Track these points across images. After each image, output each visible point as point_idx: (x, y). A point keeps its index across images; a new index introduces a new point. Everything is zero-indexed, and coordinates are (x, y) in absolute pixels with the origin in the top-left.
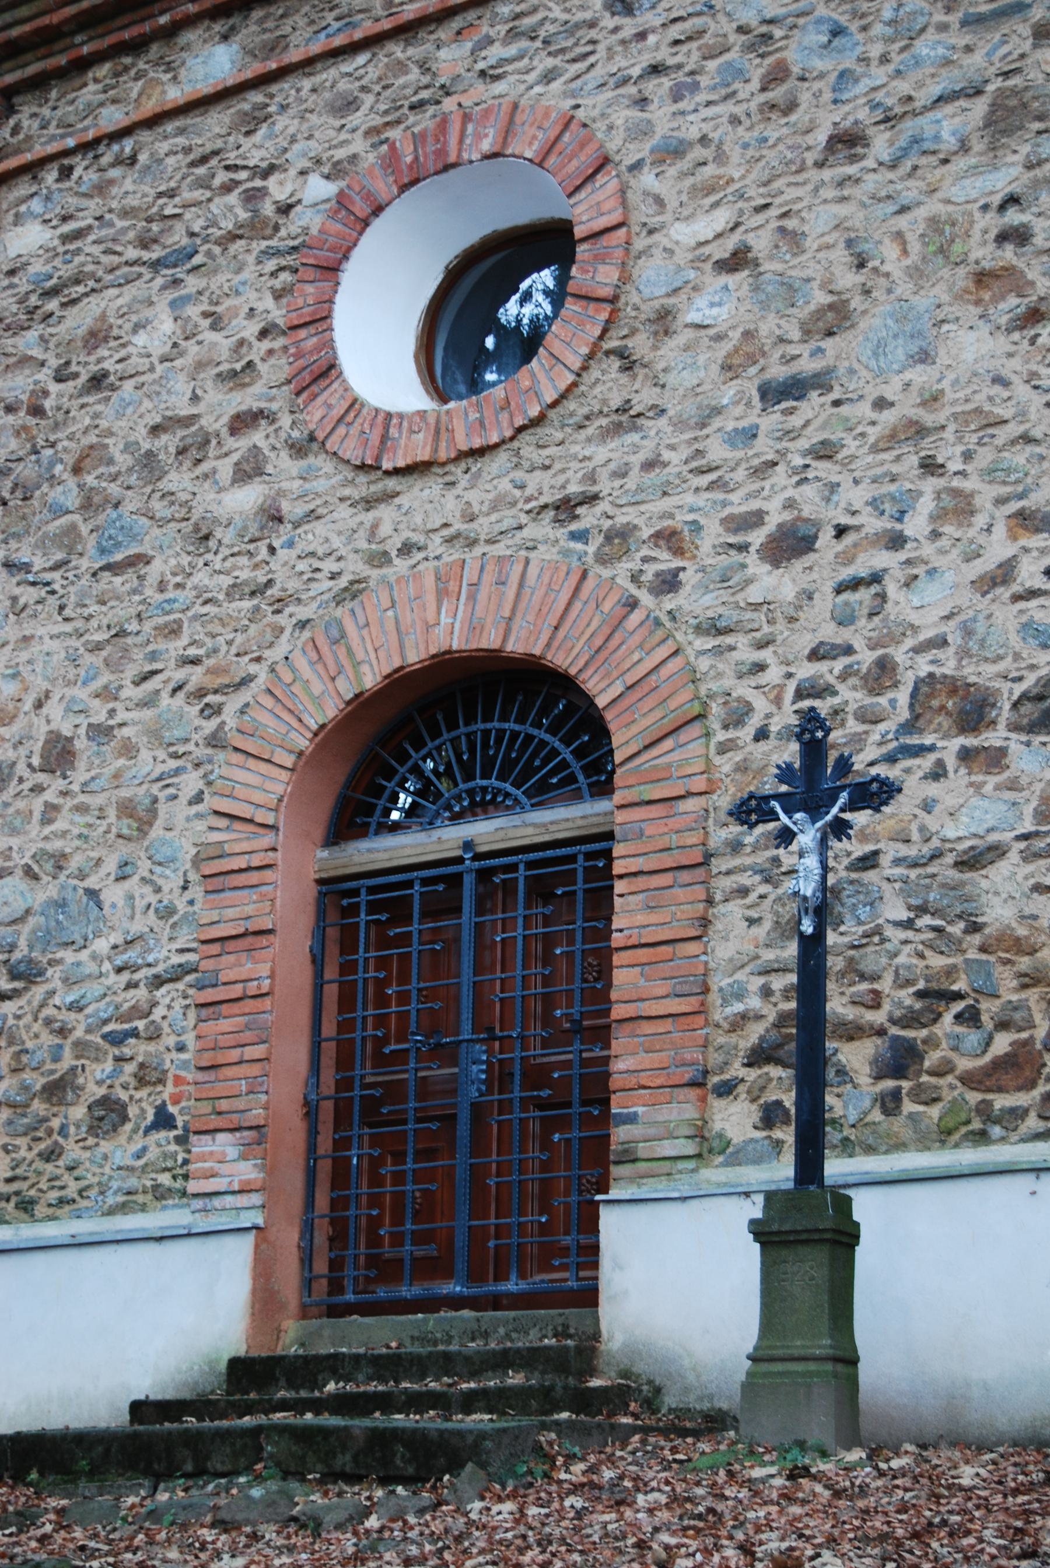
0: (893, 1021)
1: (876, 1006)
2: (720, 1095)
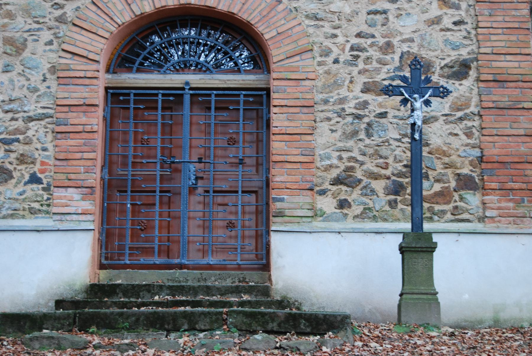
0: (393, 174)
1: (386, 168)
2: (320, 195)
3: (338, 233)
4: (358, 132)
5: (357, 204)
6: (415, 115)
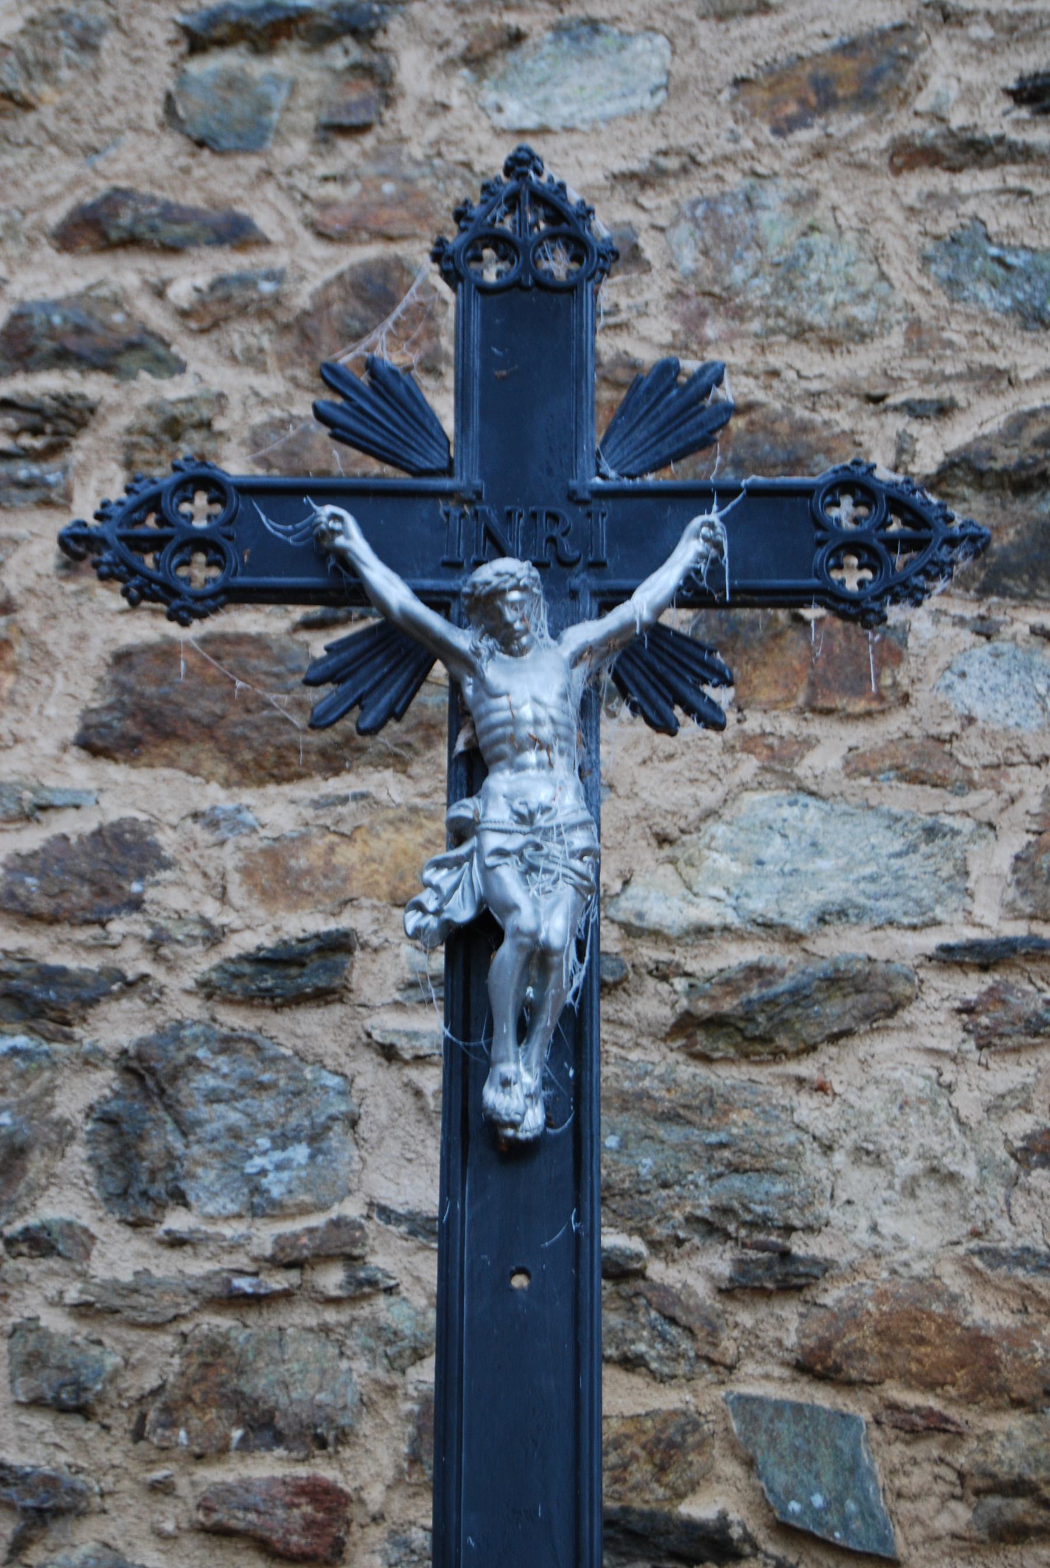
6: (498, 813)
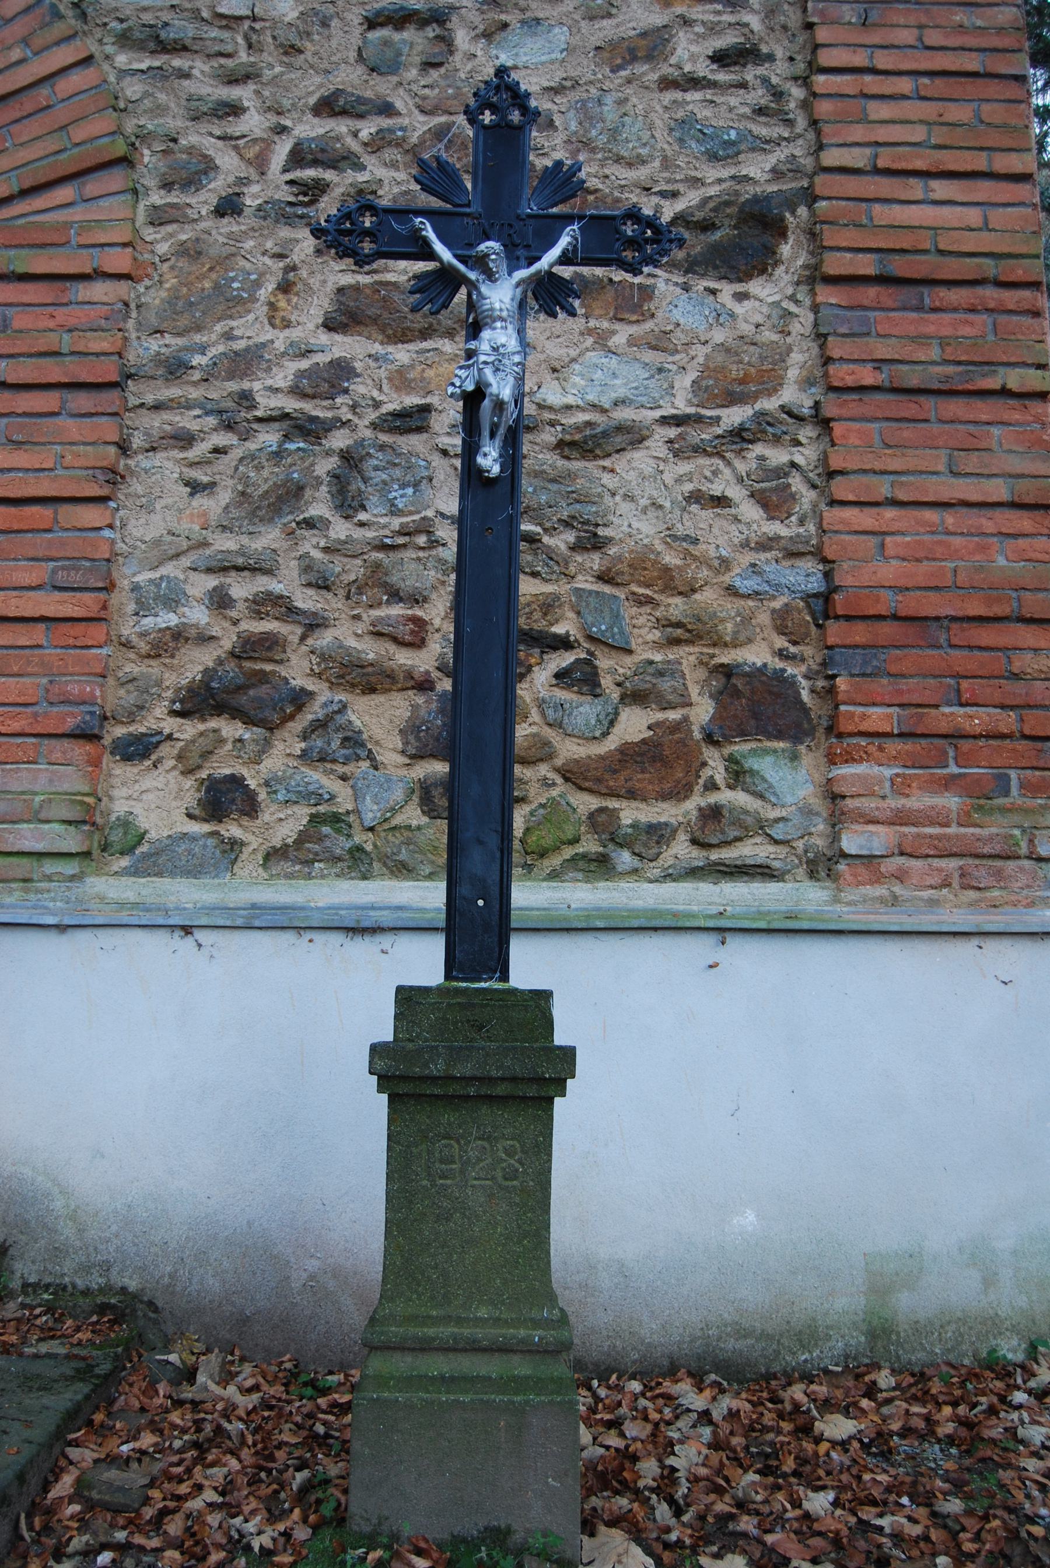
1: (418, 643)
2: (127, 758)
3: (178, 933)
4: (301, 488)
5: (280, 797)
